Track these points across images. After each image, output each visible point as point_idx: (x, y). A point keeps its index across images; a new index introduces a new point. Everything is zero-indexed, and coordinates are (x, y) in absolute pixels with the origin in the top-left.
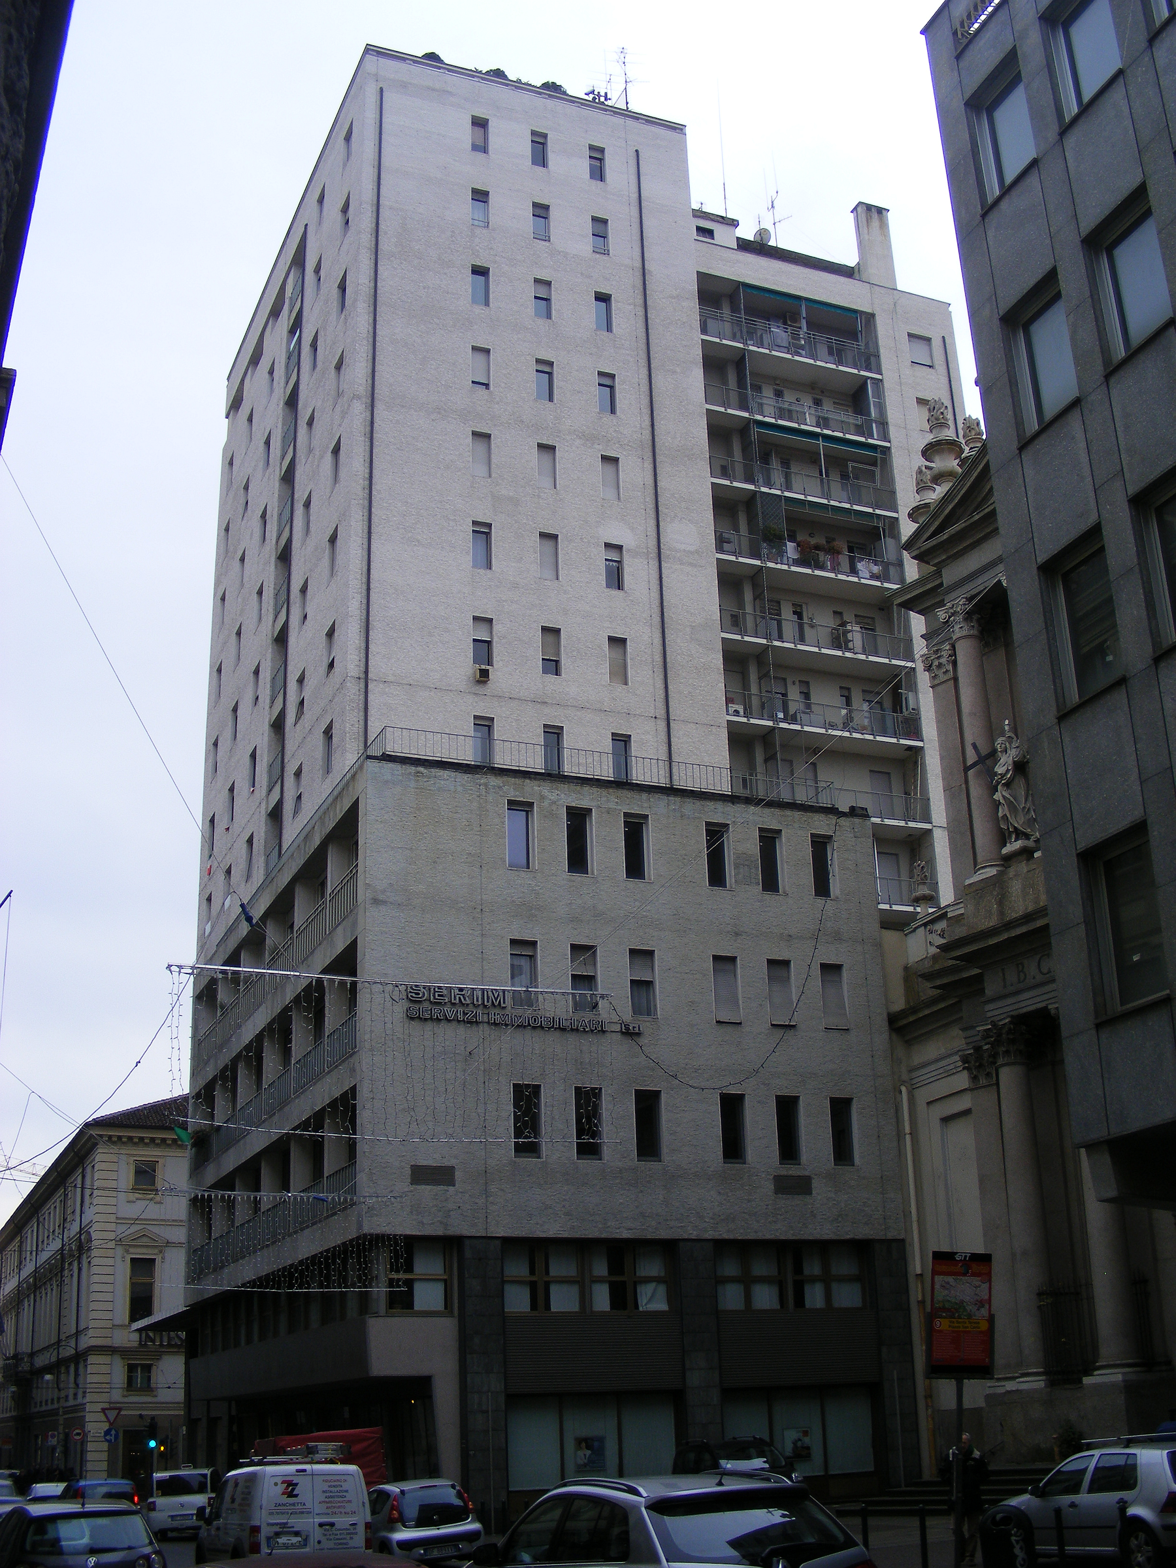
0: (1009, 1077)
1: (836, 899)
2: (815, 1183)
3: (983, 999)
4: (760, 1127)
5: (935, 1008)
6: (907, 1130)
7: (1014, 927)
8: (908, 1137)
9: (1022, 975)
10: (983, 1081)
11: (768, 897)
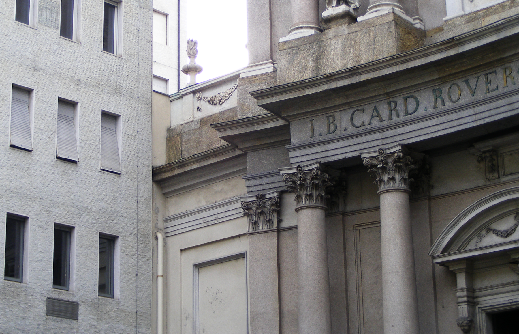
0: (306, 221)
1: (119, 57)
2: (82, 310)
3: (288, 147)
4: (38, 248)
5: (205, 163)
6: (160, 273)
7: (335, 80)
8: (160, 280)
9: (332, 127)
10: (263, 226)
11: (64, 41)
